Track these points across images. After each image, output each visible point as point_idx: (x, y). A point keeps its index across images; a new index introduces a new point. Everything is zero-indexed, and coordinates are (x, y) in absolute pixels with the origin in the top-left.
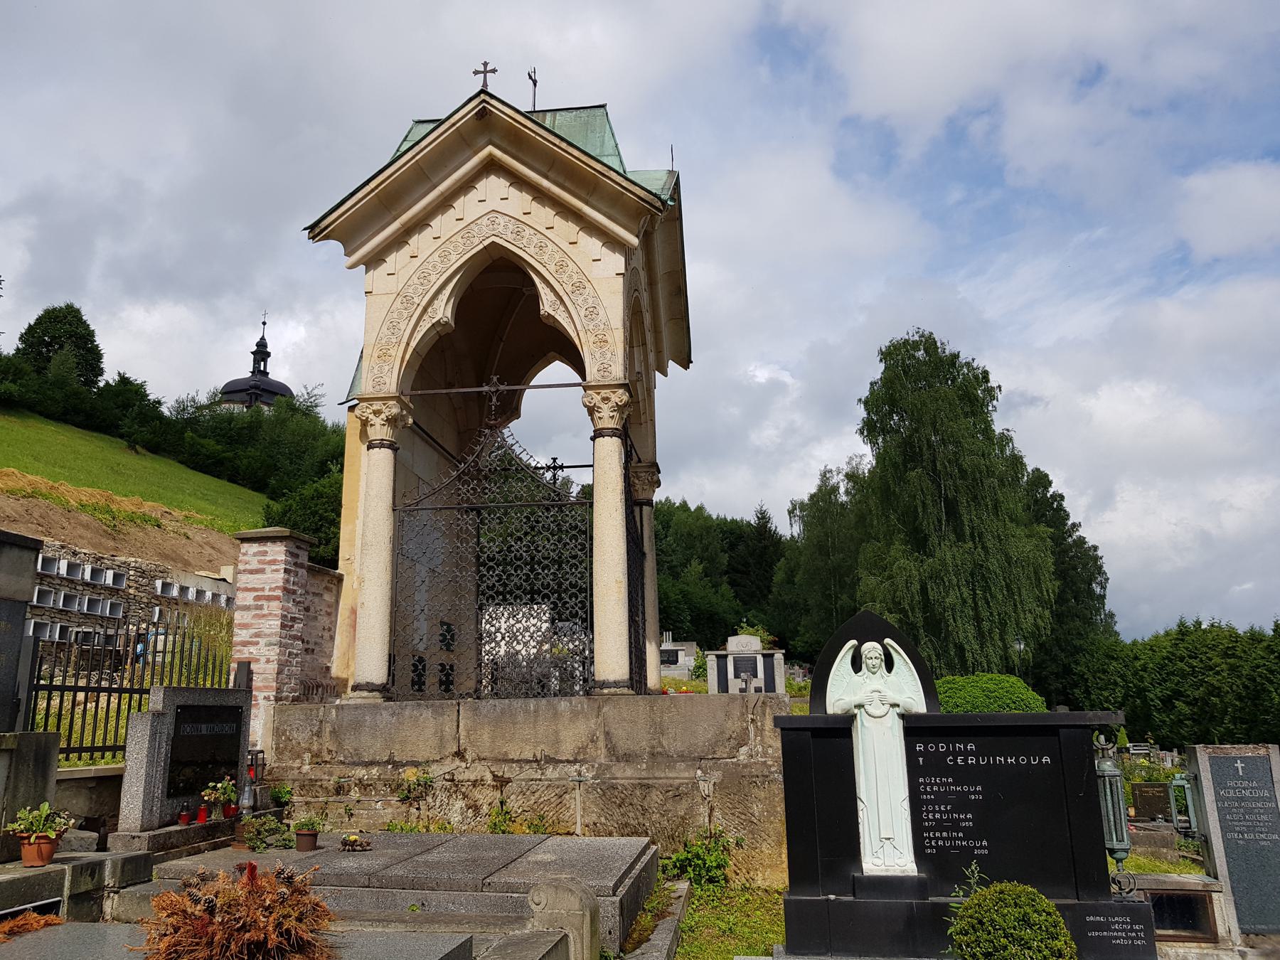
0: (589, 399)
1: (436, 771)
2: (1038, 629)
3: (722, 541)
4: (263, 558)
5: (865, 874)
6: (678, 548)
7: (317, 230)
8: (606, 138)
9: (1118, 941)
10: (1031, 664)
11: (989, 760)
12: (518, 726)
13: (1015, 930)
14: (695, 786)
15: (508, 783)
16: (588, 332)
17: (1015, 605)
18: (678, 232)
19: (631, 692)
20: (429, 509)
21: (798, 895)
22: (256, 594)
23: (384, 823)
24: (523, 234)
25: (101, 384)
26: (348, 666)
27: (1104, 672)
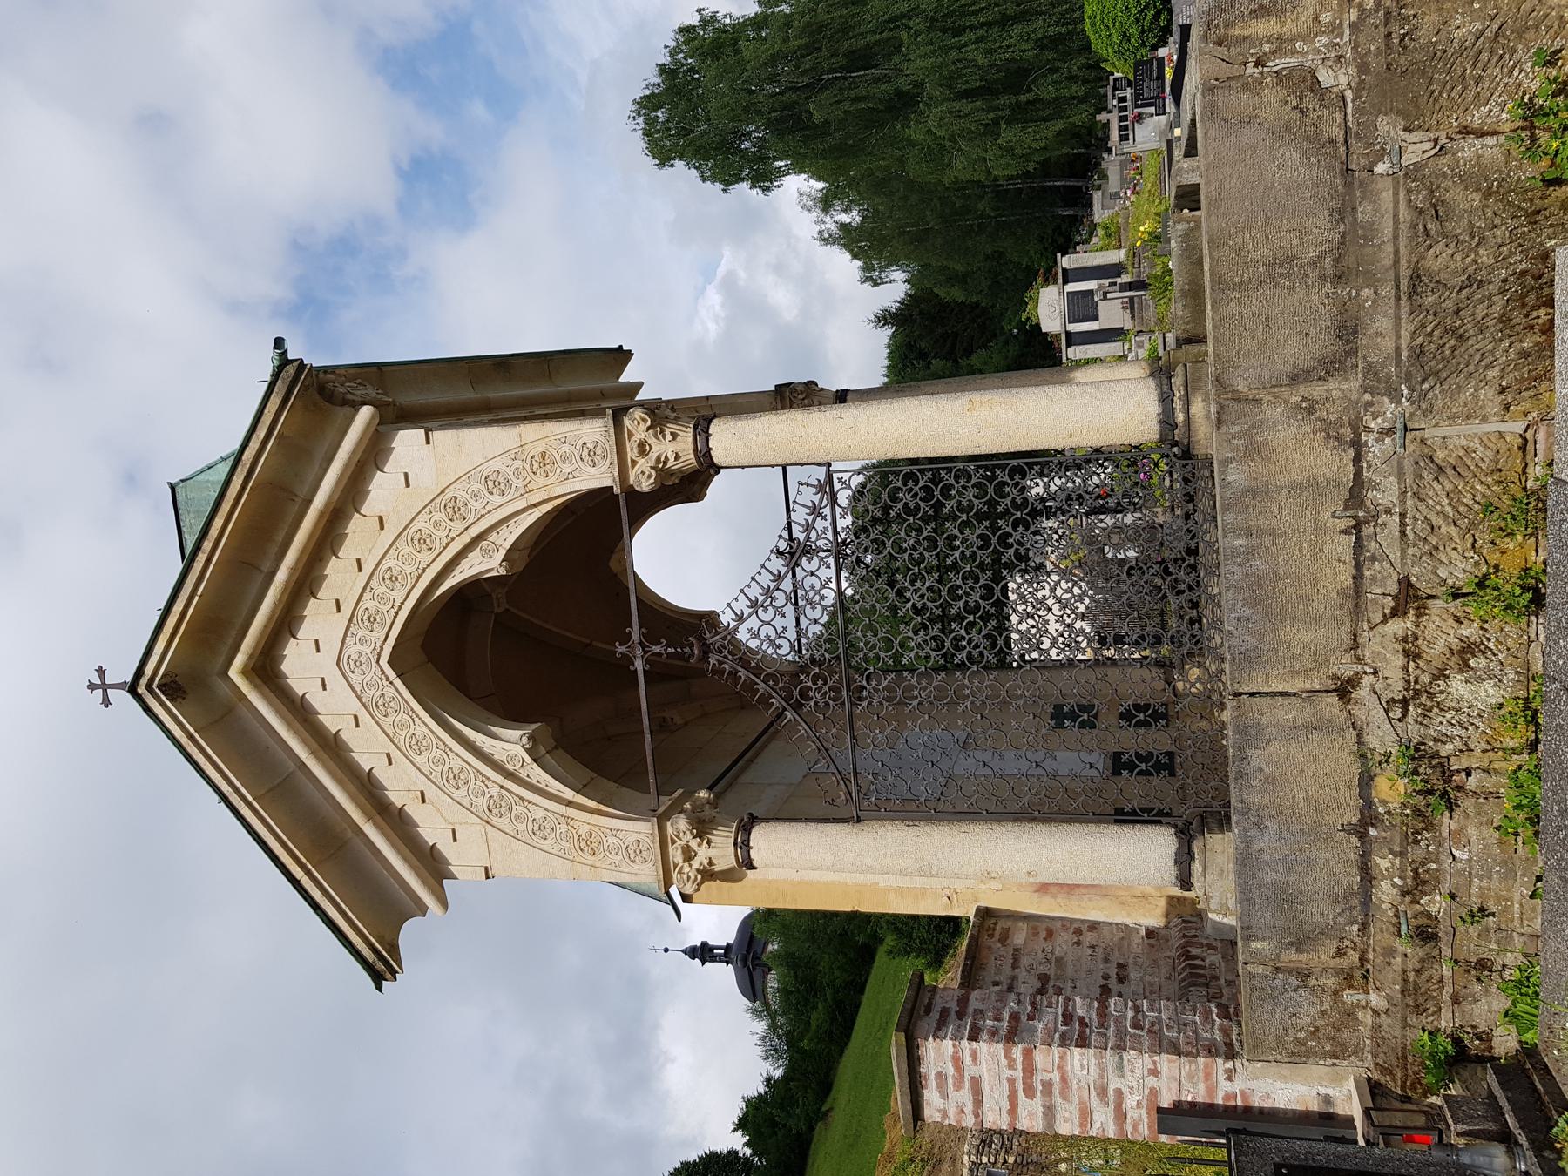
4: (950, 1081)
7: (380, 966)
12: (1282, 569)
15: (1410, 585)
16: (530, 487)
18: (394, 368)
20: (854, 756)
22: (1021, 1094)
23: (1501, 843)
24: (372, 611)
25: (748, 1152)
26: (1144, 897)
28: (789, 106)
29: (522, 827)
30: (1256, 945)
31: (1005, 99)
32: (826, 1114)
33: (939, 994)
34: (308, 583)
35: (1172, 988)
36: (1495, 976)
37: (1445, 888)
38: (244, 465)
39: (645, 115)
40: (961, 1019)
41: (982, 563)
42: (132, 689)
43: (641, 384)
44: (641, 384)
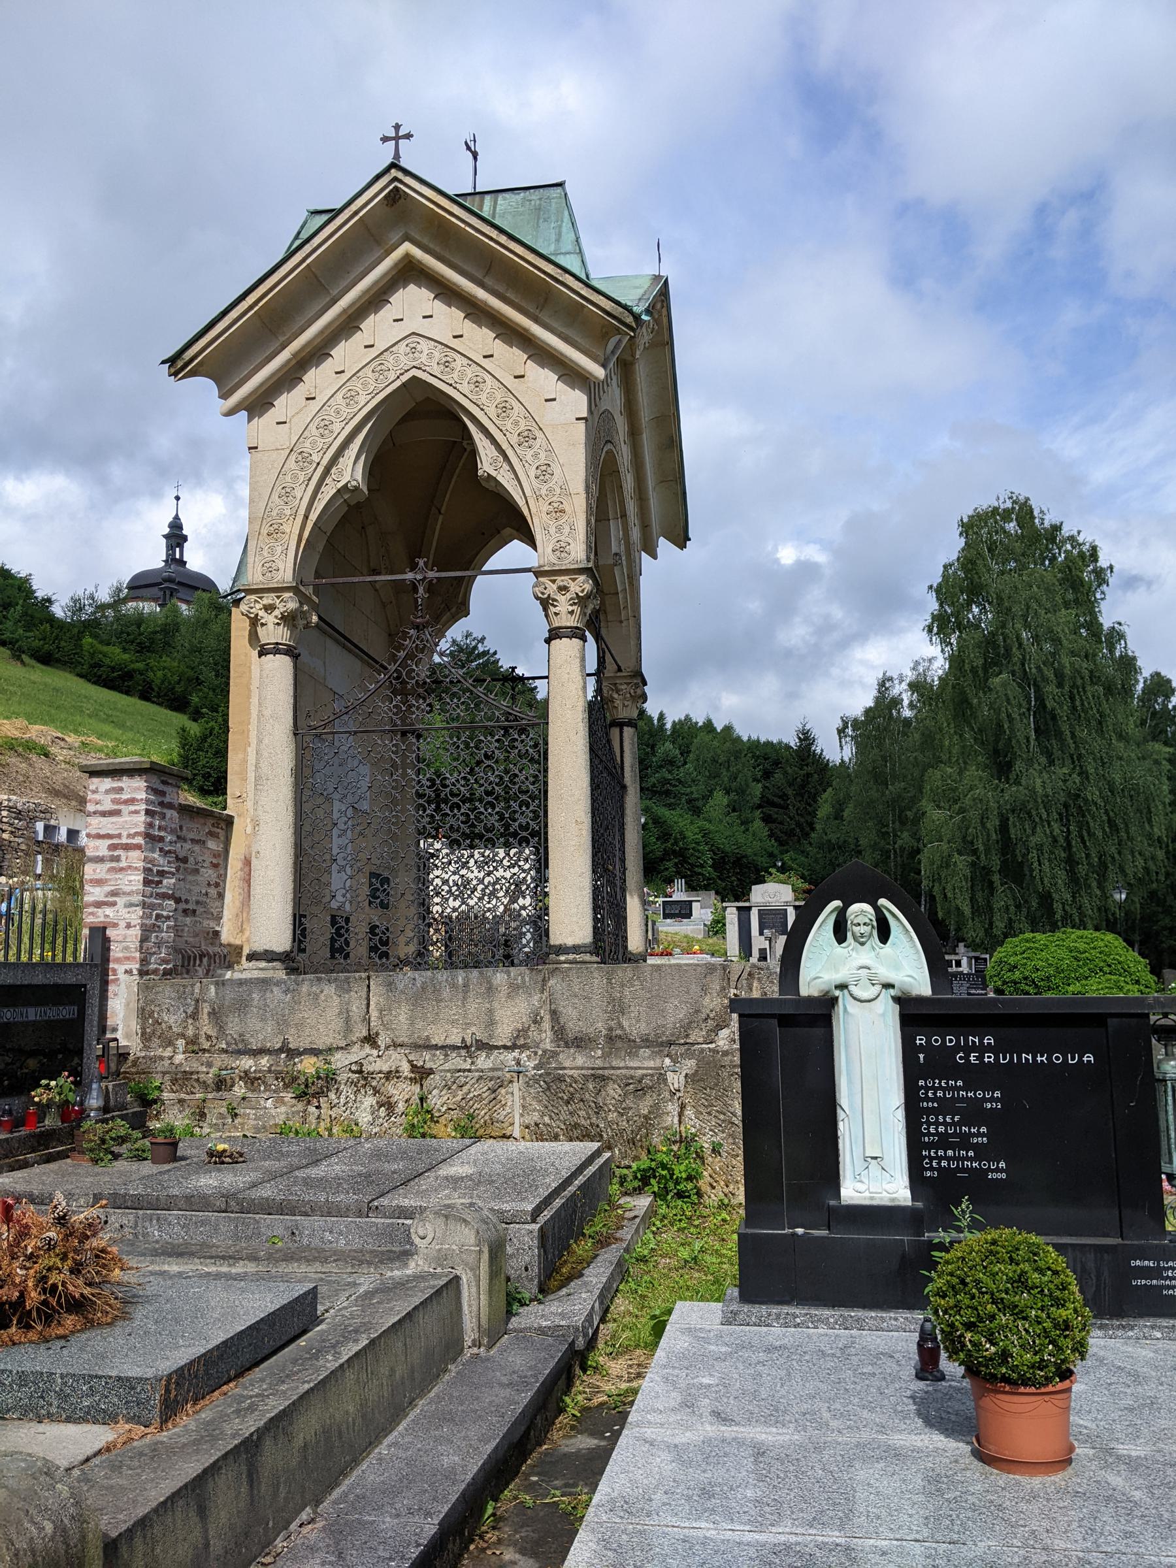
0: (541, 589)
1: (340, 1060)
4: (118, 796)
7: (180, 364)
8: (564, 229)
10: (1138, 917)
11: (1012, 1058)
13: (1007, 1293)
14: (662, 1078)
19: (595, 959)
22: (111, 842)
23: (276, 1125)
24: (453, 365)
28: (1008, 653)
30: (212, 989)
31: (996, 862)
32: (19, 658)
33: (175, 790)
36: (196, 1123)
37: (249, 1095)
39: (1013, 508)
41: (475, 826)
43: (655, 557)
44: (655, 557)
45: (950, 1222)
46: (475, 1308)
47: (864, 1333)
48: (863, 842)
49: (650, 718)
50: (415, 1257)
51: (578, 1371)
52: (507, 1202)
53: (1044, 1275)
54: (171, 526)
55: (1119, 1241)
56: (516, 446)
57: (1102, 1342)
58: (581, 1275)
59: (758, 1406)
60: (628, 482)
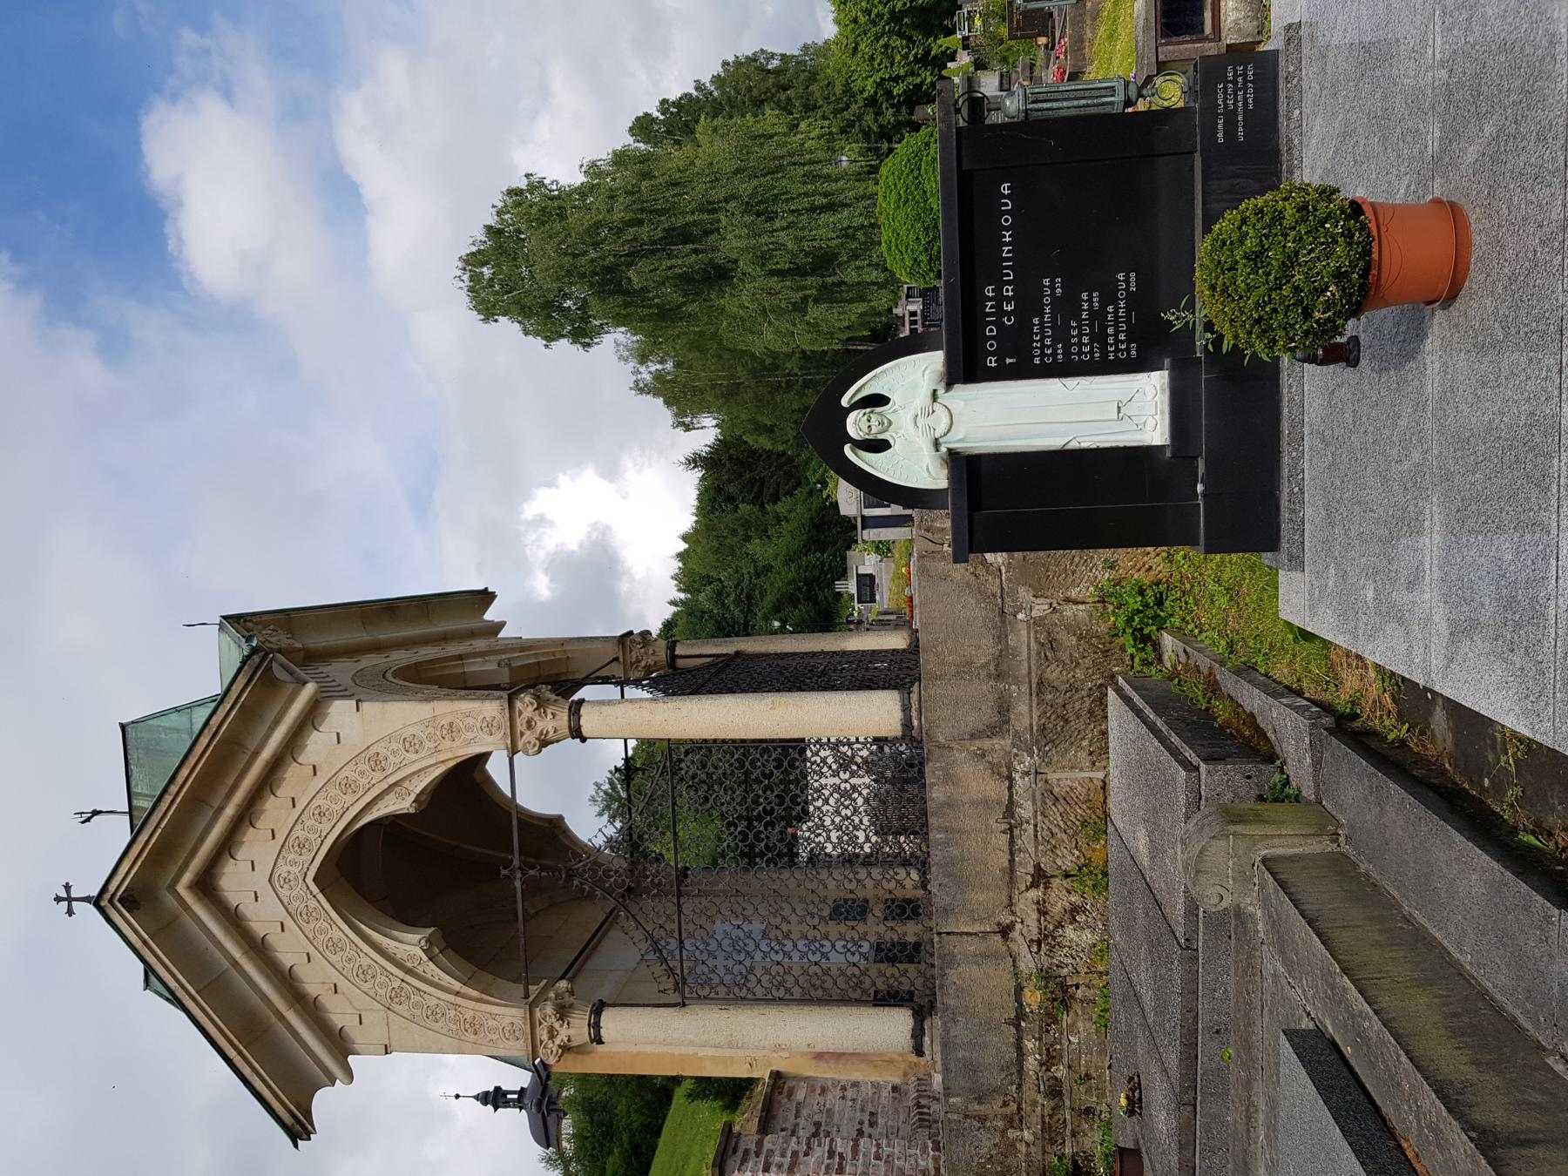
1: (1027, 963)
2: (823, 136)
3: (724, 511)
5: (1168, 443)
6: (733, 566)
8: (167, 724)
9: (1250, 101)
12: (966, 854)
13: (1269, 274)
14: (1038, 622)
16: (439, 748)
17: (795, 164)
18: (303, 614)
19: (915, 688)
21: (1198, 533)
24: (302, 840)
26: (891, 1061)
27: (872, 58)
29: (418, 1012)
31: (810, 280)
34: (248, 817)
35: (906, 1129)
38: (211, 729)
40: (757, 1157)
42: (96, 902)
45: (1188, 331)
46: (1296, 840)
47: (1306, 420)
48: (796, 406)
49: (675, 614)
50: (1242, 906)
51: (1357, 724)
52: (1177, 797)
53: (1247, 234)
54: (485, 1103)
55: (1197, 156)
56: (385, 774)
57: (1307, 172)
58: (1252, 714)
59: (1398, 539)
60: (428, 653)
